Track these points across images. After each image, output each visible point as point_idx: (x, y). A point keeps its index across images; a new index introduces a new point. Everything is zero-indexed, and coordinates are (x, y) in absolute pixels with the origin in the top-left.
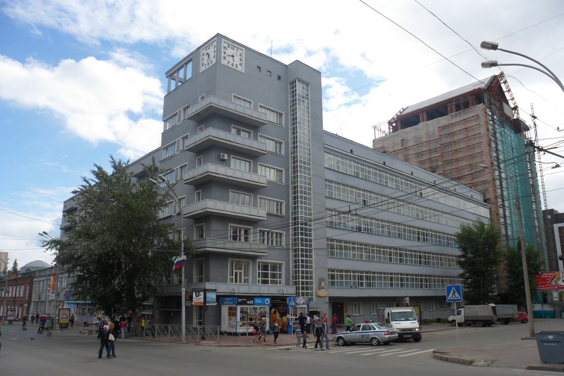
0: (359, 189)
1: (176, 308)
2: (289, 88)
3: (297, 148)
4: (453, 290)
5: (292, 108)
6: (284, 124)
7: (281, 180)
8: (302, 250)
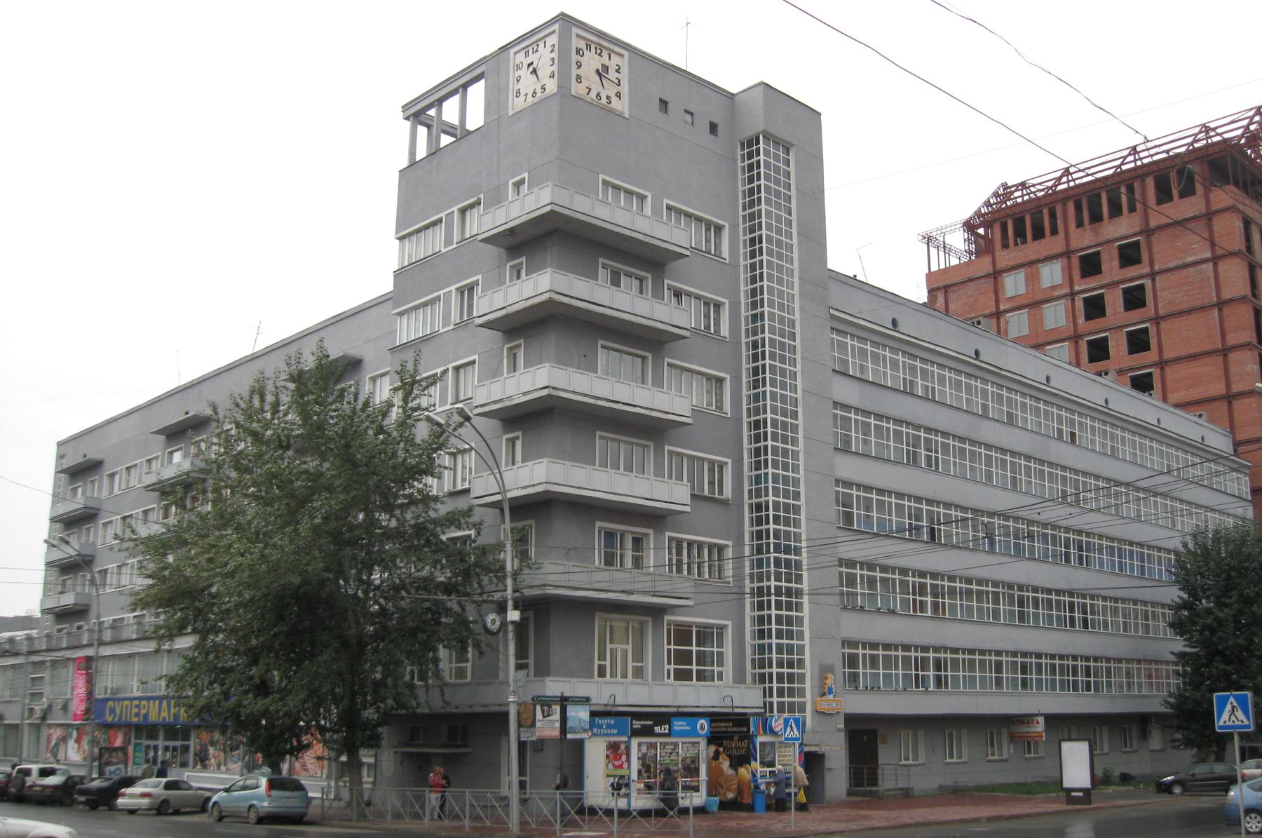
0: (917, 427)
1: (421, 746)
2: (739, 157)
3: (762, 318)
4: (1232, 703)
5: (748, 211)
6: (726, 253)
7: (720, 408)
8: (779, 591)
